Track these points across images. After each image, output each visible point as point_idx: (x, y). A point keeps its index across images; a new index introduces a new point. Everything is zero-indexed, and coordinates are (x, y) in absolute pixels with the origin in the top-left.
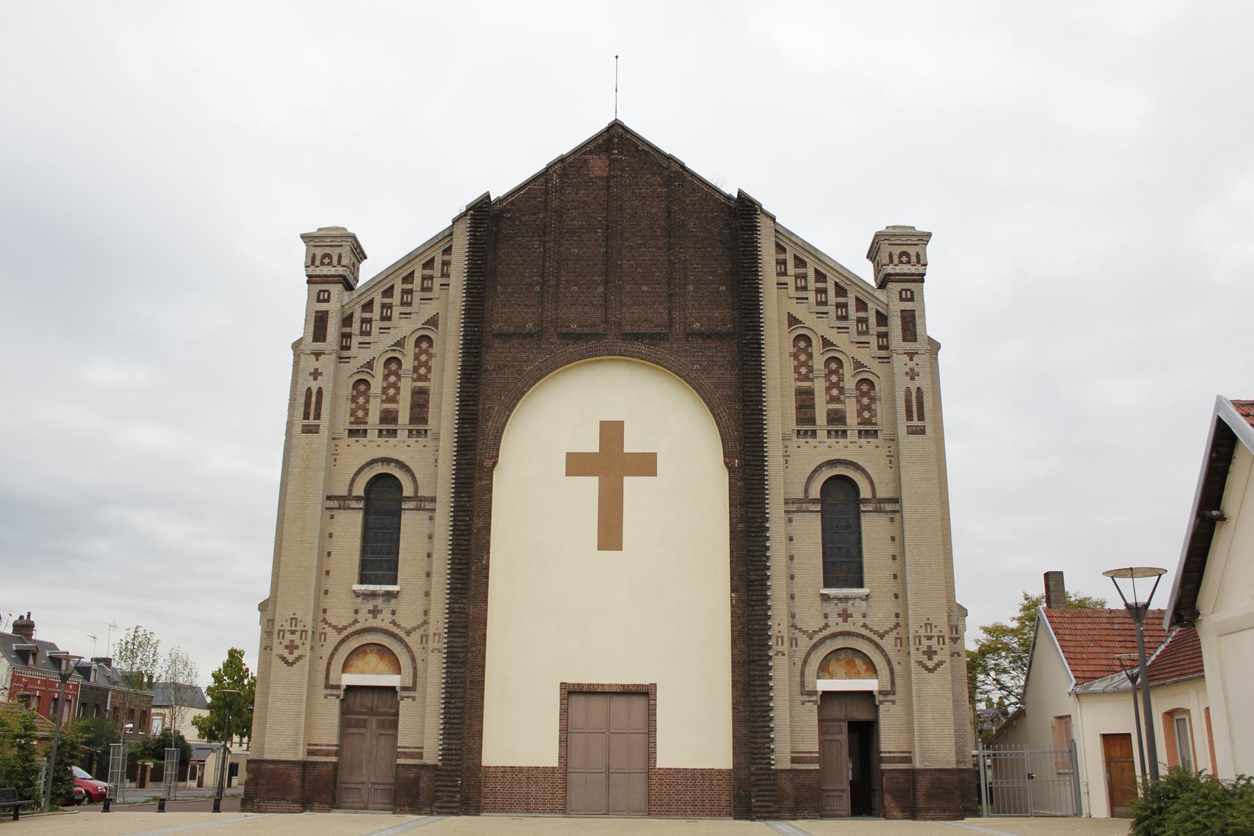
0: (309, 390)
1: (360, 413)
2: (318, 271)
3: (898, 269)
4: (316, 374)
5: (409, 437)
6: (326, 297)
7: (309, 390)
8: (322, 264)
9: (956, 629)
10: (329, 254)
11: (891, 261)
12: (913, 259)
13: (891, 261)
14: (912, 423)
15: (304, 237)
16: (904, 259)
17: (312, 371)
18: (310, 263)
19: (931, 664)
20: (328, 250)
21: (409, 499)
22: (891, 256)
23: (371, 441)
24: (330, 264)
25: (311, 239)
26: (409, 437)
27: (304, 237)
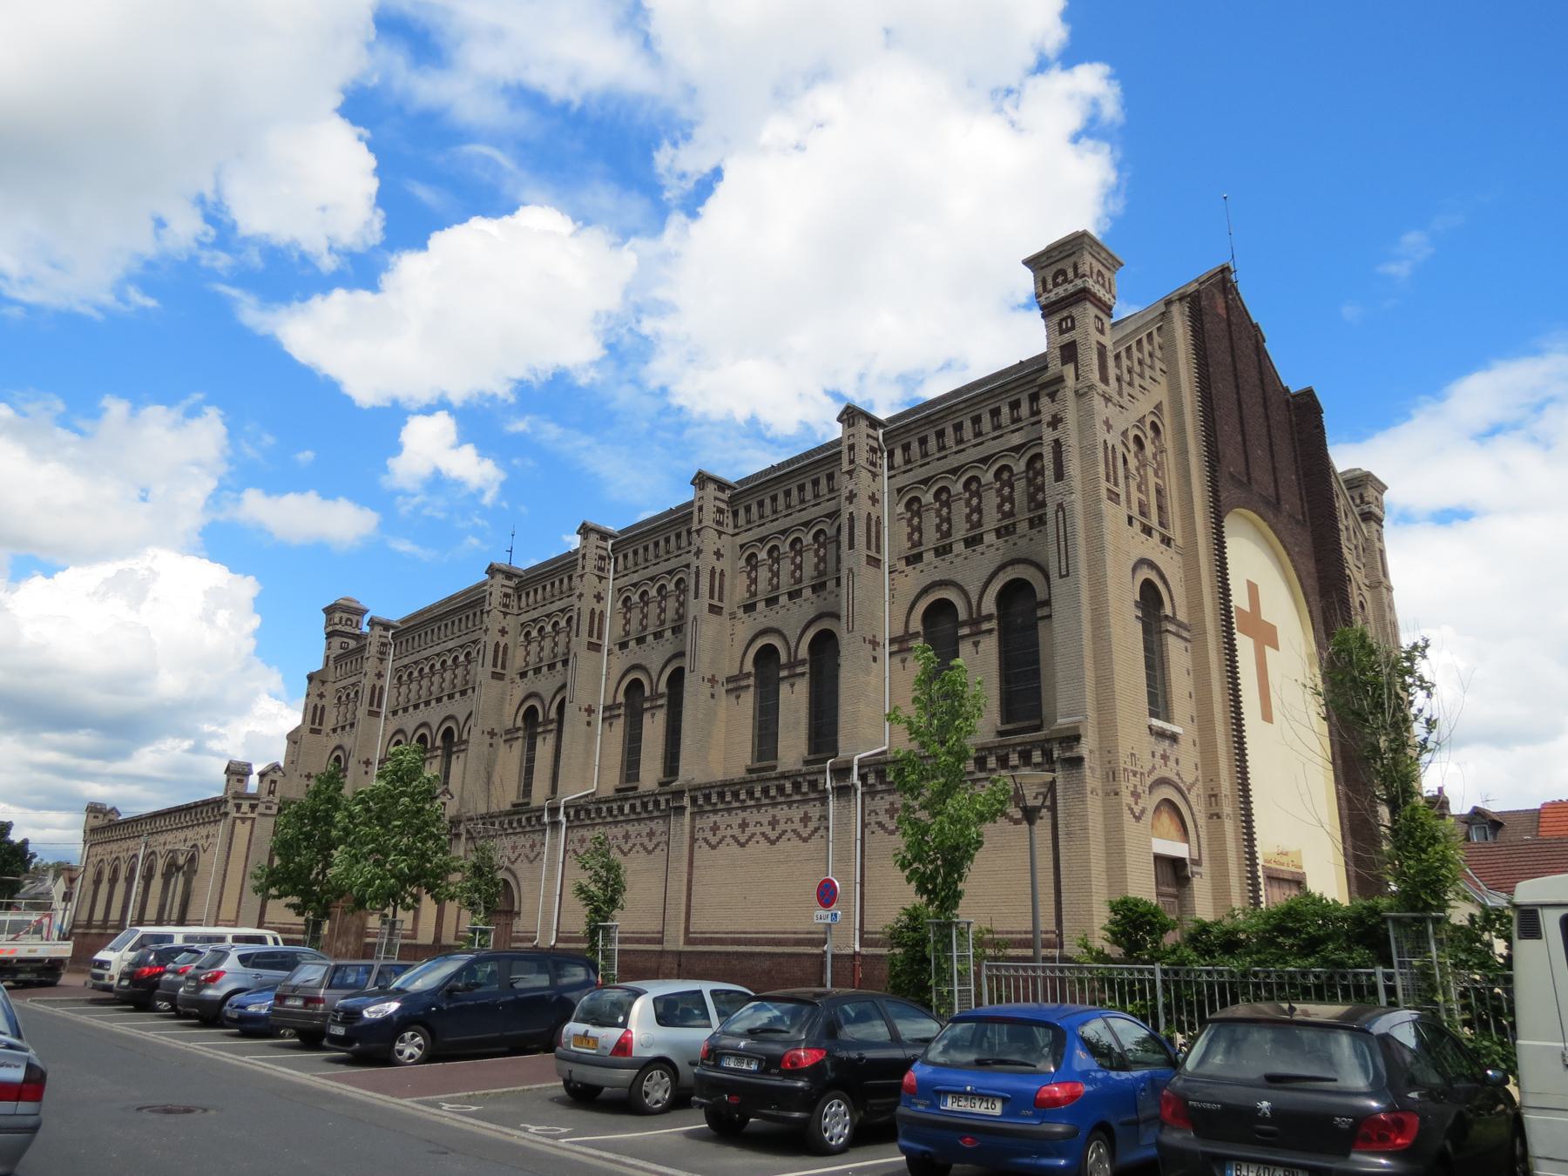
0: (316, 706)
1: (945, 527)
2: (1052, 296)
3: (343, 629)
4: (321, 696)
5: (1031, 529)
6: (1069, 325)
7: (316, 706)
8: (1056, 285)
9: (1114, 773)
10: (1061, 270)
11: (340, 622)
12: (1071, 275)
13: (340, 622)
14: (371, 709)
15: (1027, 262)
16: (349, 623)
17: (595, 600)
18: (1041, 289)
19: (773, 835)
20: (1059, 266)
21: (964, 624)
22: (341, 619)
23: (957, 556)
24: (1065, 281)
25: (1061, 249)
26: (1031, 529)
27: (1027, 262)
